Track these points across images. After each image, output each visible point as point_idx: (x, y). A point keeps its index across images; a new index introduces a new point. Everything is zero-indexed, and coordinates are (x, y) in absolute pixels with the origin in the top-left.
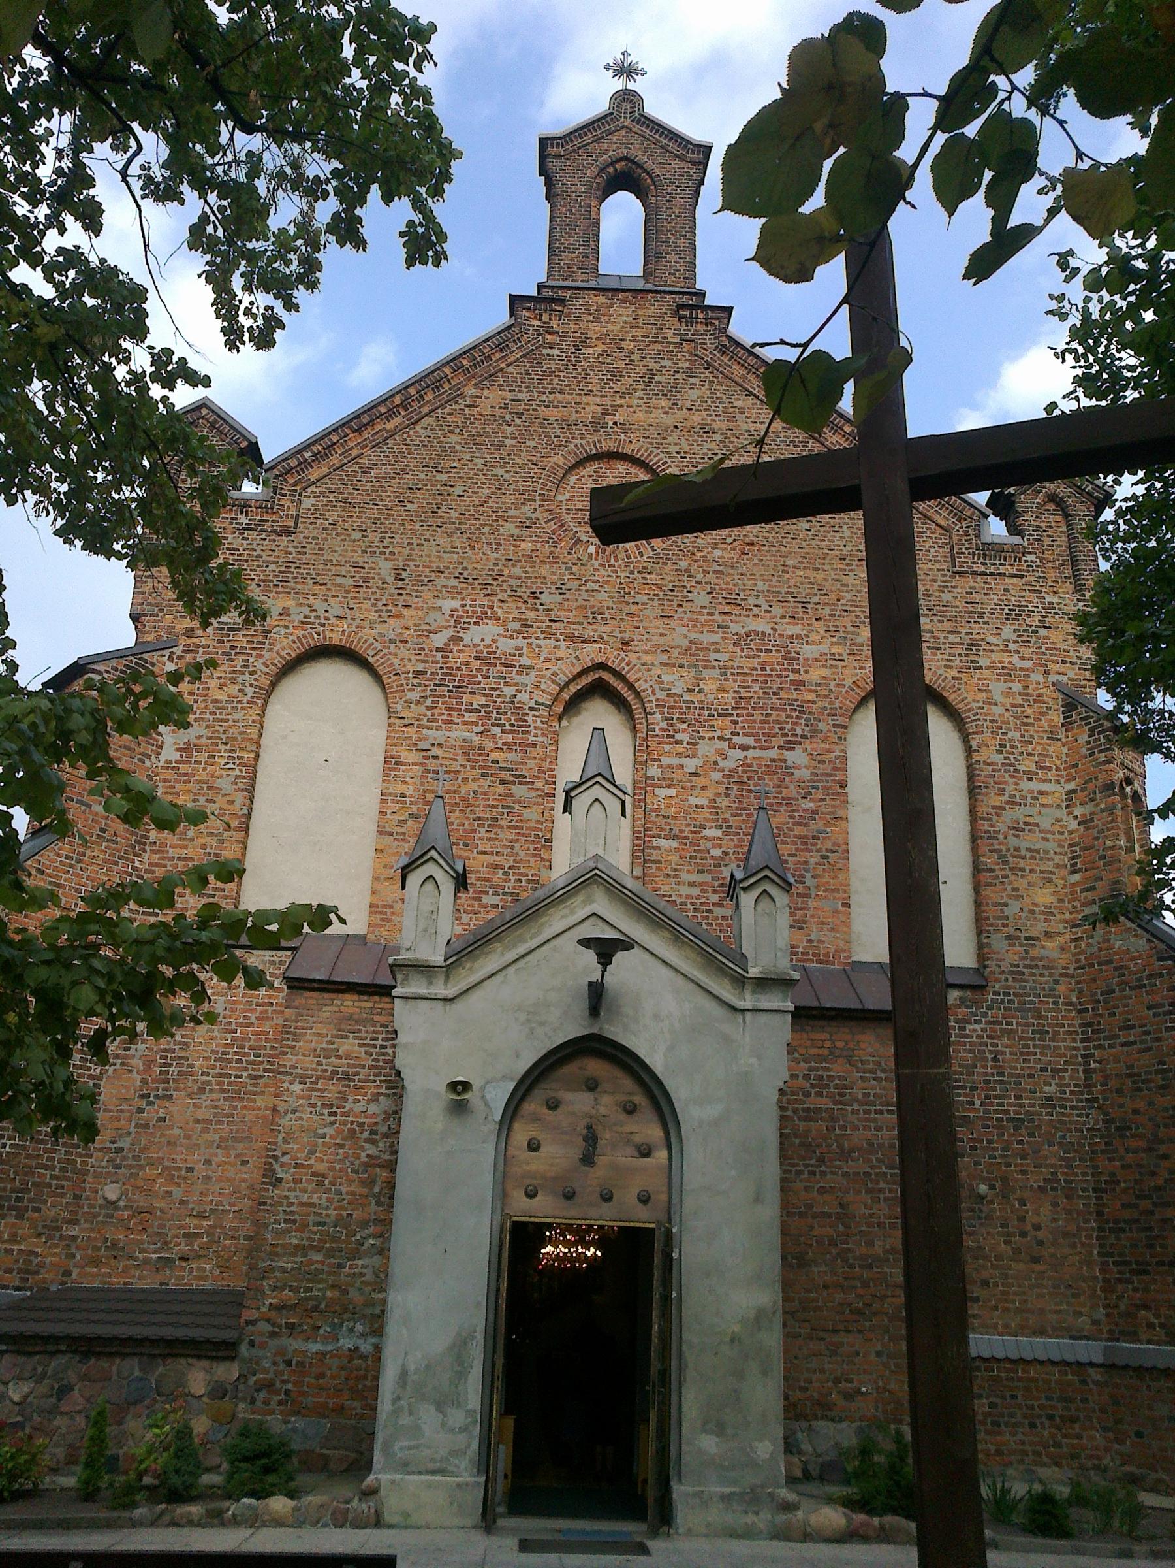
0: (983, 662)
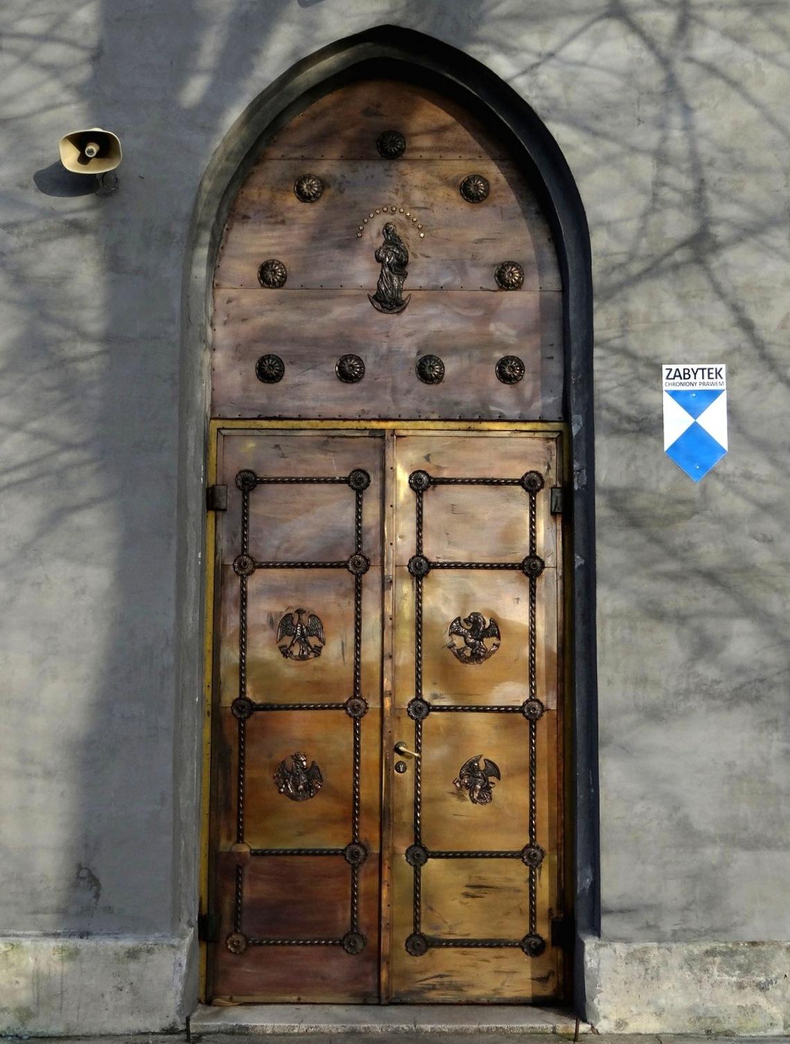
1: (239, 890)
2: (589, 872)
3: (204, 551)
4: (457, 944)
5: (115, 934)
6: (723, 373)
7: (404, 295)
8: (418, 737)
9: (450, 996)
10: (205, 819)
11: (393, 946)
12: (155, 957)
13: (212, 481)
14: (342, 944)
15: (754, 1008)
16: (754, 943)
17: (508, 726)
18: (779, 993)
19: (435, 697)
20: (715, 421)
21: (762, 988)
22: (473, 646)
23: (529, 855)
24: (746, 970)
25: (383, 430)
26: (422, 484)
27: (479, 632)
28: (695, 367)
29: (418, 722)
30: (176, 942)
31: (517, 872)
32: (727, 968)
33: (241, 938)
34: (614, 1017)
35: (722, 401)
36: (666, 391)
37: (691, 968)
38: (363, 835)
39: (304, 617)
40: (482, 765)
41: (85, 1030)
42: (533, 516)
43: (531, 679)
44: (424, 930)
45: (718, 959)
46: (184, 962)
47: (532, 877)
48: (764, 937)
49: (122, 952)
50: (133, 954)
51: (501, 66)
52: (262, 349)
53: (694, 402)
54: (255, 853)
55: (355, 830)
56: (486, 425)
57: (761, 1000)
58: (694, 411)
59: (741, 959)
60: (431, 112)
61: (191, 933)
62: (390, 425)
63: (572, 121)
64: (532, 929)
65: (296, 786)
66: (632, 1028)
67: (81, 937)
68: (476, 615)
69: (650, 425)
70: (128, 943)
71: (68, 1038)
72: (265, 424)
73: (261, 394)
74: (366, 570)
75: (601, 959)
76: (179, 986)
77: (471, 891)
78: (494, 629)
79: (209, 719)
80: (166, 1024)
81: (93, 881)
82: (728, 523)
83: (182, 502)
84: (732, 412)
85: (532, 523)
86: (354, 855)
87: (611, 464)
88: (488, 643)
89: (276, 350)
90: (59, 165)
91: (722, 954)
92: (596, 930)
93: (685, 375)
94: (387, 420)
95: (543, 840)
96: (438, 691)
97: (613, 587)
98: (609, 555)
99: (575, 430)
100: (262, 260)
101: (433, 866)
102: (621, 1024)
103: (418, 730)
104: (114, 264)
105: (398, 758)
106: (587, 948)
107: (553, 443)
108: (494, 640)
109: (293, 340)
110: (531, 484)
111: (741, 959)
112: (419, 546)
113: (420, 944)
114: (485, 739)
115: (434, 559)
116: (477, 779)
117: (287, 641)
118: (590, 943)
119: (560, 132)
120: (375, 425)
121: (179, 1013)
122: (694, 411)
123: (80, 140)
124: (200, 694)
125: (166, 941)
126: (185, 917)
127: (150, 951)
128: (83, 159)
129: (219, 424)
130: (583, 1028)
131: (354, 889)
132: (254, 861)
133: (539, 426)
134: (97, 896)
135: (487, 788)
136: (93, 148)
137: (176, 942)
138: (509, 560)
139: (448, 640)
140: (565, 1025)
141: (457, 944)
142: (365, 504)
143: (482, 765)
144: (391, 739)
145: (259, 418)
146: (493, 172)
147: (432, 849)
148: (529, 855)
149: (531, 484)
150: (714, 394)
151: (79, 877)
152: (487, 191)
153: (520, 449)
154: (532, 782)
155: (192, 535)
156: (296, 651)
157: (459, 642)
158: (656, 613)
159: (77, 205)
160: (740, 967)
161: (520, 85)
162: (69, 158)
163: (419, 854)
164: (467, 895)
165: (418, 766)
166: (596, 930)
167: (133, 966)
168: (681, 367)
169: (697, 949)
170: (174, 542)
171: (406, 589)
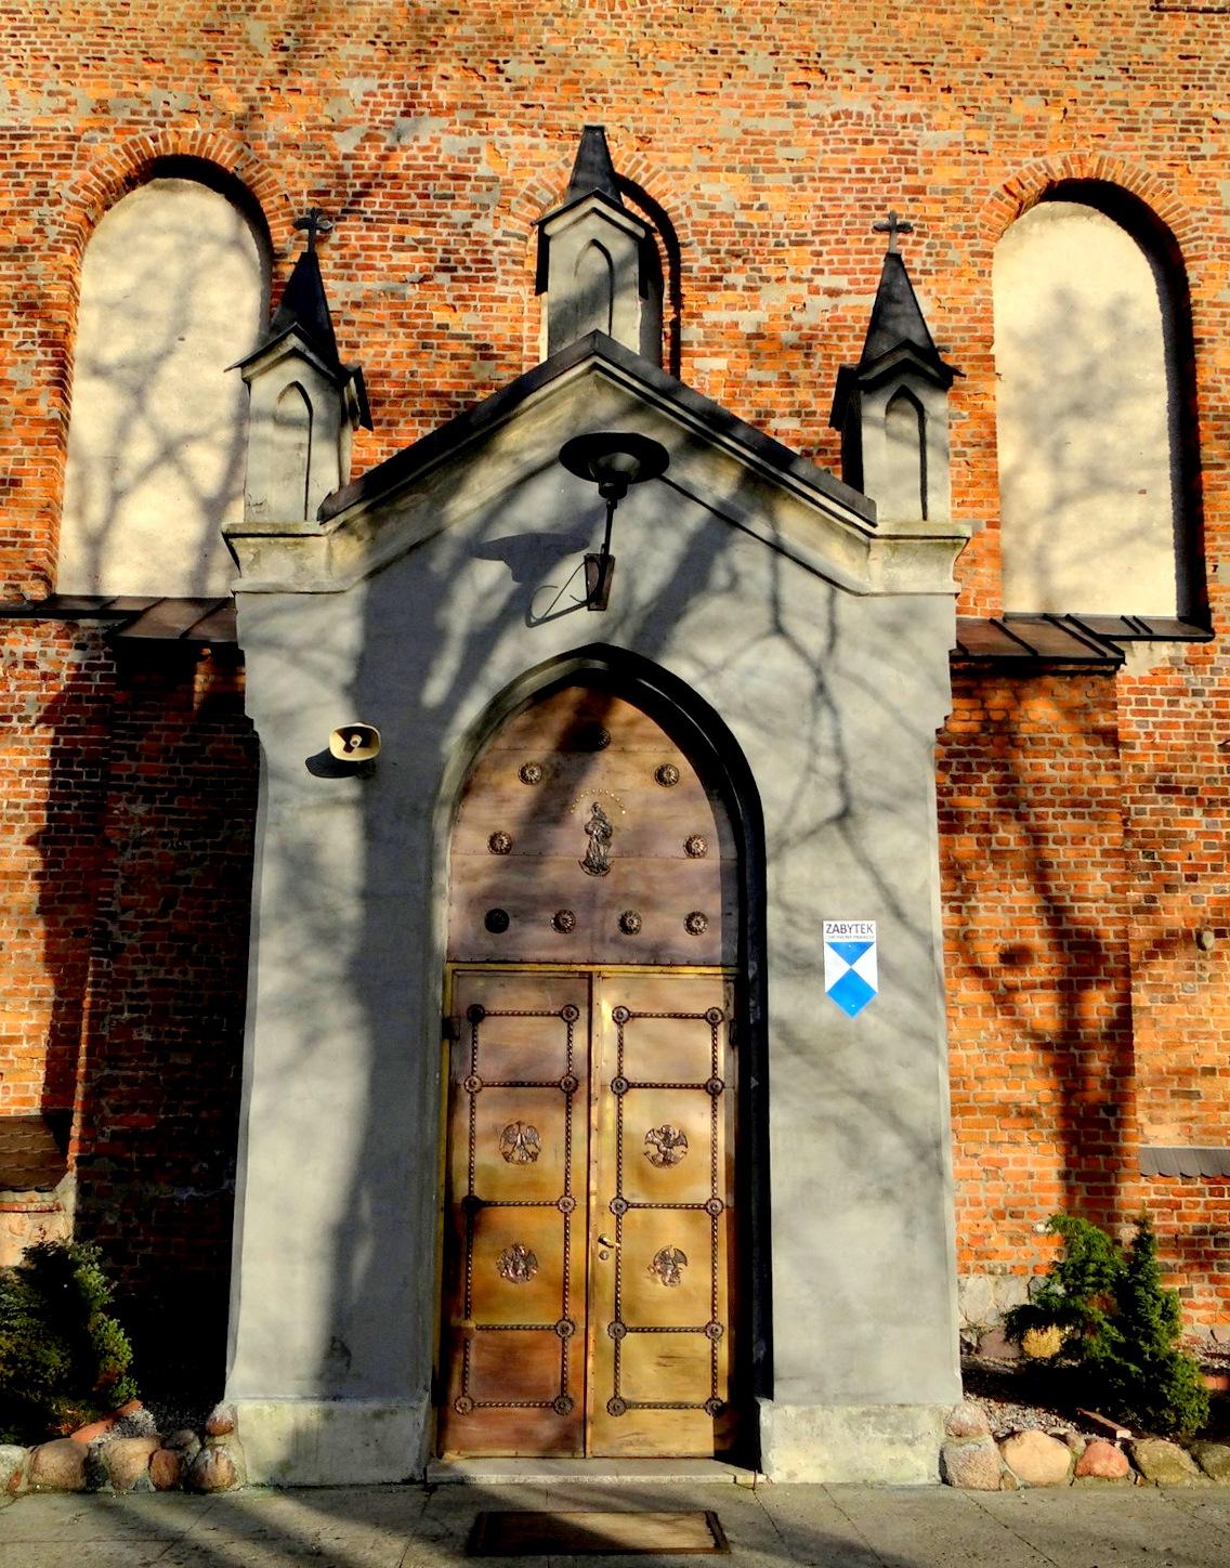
0: (1207, 149)
1: (466, 1359)
2: (763, 1344)
3: (441, 1072)
4: (650, 1406)
5: (363, 1398)
6: (874, 928)
7: (608, 862)
8: (618, 1230)
9: (645, 1451)
10: (439, 1300)
11: (597, 1408)
12: (398, 1417)
13: (448, 1014)
14: (553, 1406)
15: (902, 1461)
16: (902, 1406)
17: (694, 1221)
18: (923, 1447)
19: (633, 1196)
20: (867, 968)
21: (910, 1443)
22: (665, 1153)
23: (709, 1330)
24: (897, 1429)
25: (590, 973)
26: (622, 1017)
27: (670, 1141)
28: (850, 923)
29: (618, 1217)
30: (415, 1404)
31: (702, 1344)
32: (879, 1428)
33: (468, 1401)
34: (785, 1469)
35: (873, 949)
36: (834, 946)
37: (850, 1427)
38: (571, 1313)
39: (523, 1128)
40: (672, 1254)
41: (336, 1481)
42: (714, 1045)
43: (713, 1181)
44: (623, 1394)
45: (872, 1419)
46: (422, 1421)
47: (714, 1348)
48: (910, 1401)
49: (369, 1413)
50: (378, 1415)
51: (684, 671)
52: (492, 905)
53: (853, 952)
54: (480, 1328)
55: (564, 1309)
56: (681, 969)
57: (908, 1453)
58: (851, 960)
59: (892, 1419)
60: (162, 216)
61: (427, 1397)
62: (597, 968)
63: (746, 714)
64: (714, 1394)
65: (515, 1270)
66: (800, 1478)
67: (334, 1399)
68: (668, 1127)
69: (814, 968)
70: (374, 1405)
71: (322, 1487)
72: (493, 967)
73: (488, 942)
74: (576, 1088)
75: (771, 1417)
76: (417, 1442)
77: (664, 1361)
78: (682, 1140)
79: (442, 1215)
80: (406, 1475)
81: (346, 1352)
82: (875, 1050)
83: (424, 1029)
84: (882, 963)
85: (714, 1051)
86: (563, 1329)
87: (782, 999)
88: (677, 1150)
89: (503, 905)
90: (328, 752)
91: (876, 1415)
92: (770, 1396)
93: (842, 930)
94: (593, 964)
95: (723, 1317)
96: (635, 1191)
97: (785, 1103)
98: (781, 1070)
99: (751, 974)
100: (491, 833)
101: (630, 1341)
102: (791, 1475)
103: (618, 1224)
104: (371, 832)
105: (602, 1247)
106: (762, 1410)
107: (731, 985)
108: (683, 1148)
109: (516, 897)
110: (711, 1019)
111: (892, 1419)
112: (620, 1068)
113: (619, 1406)
114: (674, 1231)
115: (631, 1080)
116: (669, 1263)
117: (509, 1148)
118: (765, 1407)
119: (740, 730)
120: (583, 968)
121: (418, 1466)
122: (851, 960)
123: (346, 734)
124: (436, 1195)
125: (407, 1405)
126: (422, 1382)
127: (392, 1412)
128: (348, 748)
129: (455, 966)
130: (761, 1478)
131: (564, 1359)
132: (478, 1334)
133: (719, 970)
134: (348, 1365)
135: (676, 1274)
136: (357, 739)
137: (415, 1404)
138: (696, 1081)
139: (644, 1148)
140: (746, 1477)
141: (650, 1406)
142: (574, 1033)
143: (672, 1254)
144: (596, 1232)
145: (488, 961)
146: (681, 762)
147: (630, 1325)
148: (709, 1330)
149: (711, 1019)
150: (864, 947)
151: (333, 1349)
152: (677, 777)
153: (706, 990)
154: (714, 1268)
155: (432, 1060)
156: (516, 1156)
157: (653, 1150)
158: (823, 1123)
159: (346, 787)
160: (891, 1425)
161: (704, 690)
162: (337, 748)
163: (619, 1329)
164: (659, 1364)
165: (618, 1255)
166: (770, 1396)
167: (378, 1425)
168: (839, 923)
169: (855, 1410)
170: (417, 1065)
171: (610, 1102)
